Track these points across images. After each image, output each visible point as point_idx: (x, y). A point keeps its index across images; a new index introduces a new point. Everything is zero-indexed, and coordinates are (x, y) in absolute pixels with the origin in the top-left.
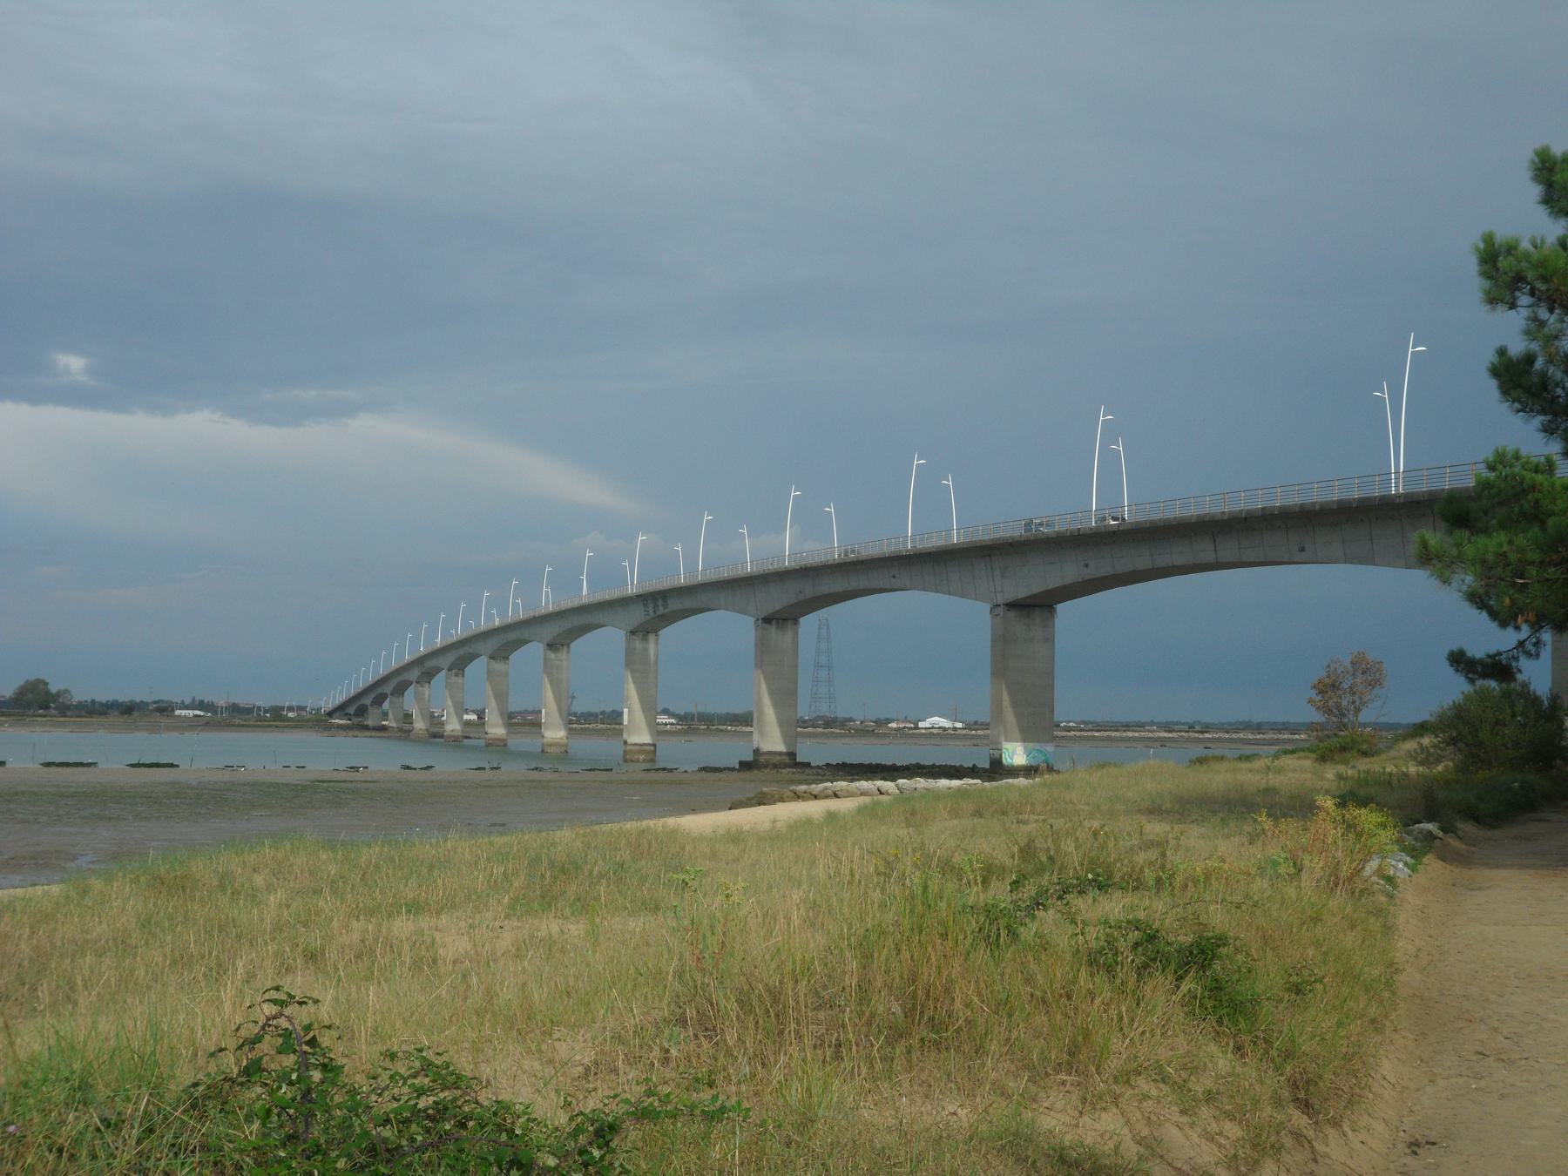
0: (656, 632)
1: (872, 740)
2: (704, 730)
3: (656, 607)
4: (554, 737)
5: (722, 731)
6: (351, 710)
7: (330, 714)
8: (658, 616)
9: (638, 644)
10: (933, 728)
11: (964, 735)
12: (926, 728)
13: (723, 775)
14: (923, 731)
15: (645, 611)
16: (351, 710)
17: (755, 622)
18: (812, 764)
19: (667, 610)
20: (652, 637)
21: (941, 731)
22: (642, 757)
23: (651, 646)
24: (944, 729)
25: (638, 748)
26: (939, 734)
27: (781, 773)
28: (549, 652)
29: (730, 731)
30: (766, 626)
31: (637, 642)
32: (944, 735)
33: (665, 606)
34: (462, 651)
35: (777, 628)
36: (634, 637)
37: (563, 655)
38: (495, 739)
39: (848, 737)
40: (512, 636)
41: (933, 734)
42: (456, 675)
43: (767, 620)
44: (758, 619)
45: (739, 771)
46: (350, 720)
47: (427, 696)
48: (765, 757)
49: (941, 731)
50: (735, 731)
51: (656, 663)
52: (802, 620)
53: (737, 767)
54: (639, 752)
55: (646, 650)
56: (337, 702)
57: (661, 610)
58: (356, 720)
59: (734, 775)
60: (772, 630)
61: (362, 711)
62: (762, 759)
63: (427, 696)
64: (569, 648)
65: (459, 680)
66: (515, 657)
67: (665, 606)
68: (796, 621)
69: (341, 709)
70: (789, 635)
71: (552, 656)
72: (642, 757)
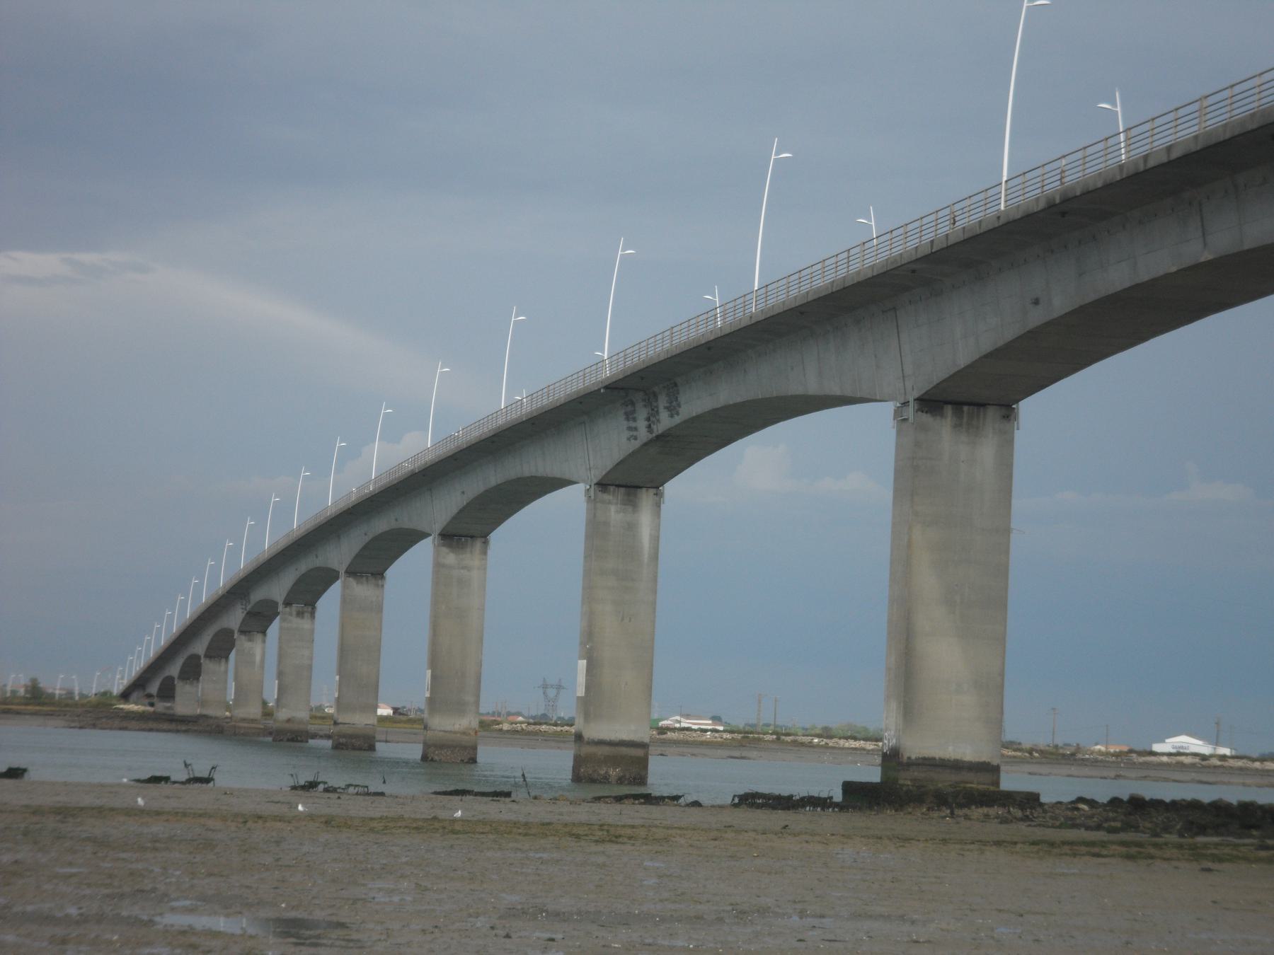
0: (656, 485)
1: (1074, 770)
2: (772, 741)
3: (651, 419)
4: (448, 728)
5: (802, 744)
6: (154, 688)
7: (125, 696)
8: (658, 437)
9: (614, 513)
10: (1179, 754)
11: (1241, 769)
12: (1170, 754)
13: (797, 819)
14: (1165, 759)
15: (630, 429)
16: (154, 688)
17: (897, 413)
18: (1043, 799)
19: (677, 420)
20: (646, 498)
21: (1197, 760)
22: (614, 773)
23: (645, 519)
24: (1204, 757)
25: (606, 750)
26: (1193, 765)
27: (967, 817)
28: (445, 550)
29: (818, 746)
30: (926, 418)
31: (613, 508)
32: (1204, 767)
33: (673, 410)
34: (304, 566)
35: (957, 426)
36: (606, 497)
37: (471, 558)
38: (351, 736)
39: (1028, 763)
40: (381, 525)
41: (1182, 765)
42: (300, 614)
43: (931, 403)
44: (905, 404)
45: (841, 807)
46: (152, 705)
47: (258, 658)
48: (916, 773)
49: (1197, 760)
50: (826, 747)
51: (655, 556)
52: (1029, 408)
53: (838, 797)
54: (614, 761)
55: (632, 527)
56: (133, 674)
57: (665, 422)
58: (161, 706)
59: (829, 821)
60: (944, 429)
61: (167, 692)
62: (905, 779)
63: (258, 658)
64: (486, 543)
65: (304, 624)
66: (395, 572)
67: (673, 410)
68: (1007, 411)
69: (138, 685)
70: (987, 450)
71: (450, 558)
72: (614, 773)
